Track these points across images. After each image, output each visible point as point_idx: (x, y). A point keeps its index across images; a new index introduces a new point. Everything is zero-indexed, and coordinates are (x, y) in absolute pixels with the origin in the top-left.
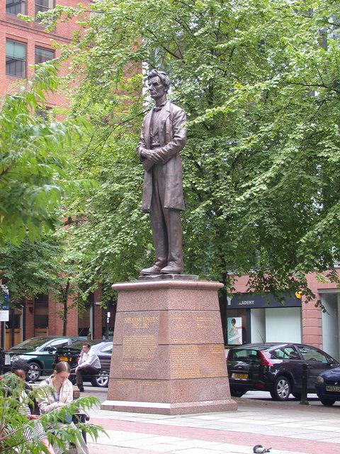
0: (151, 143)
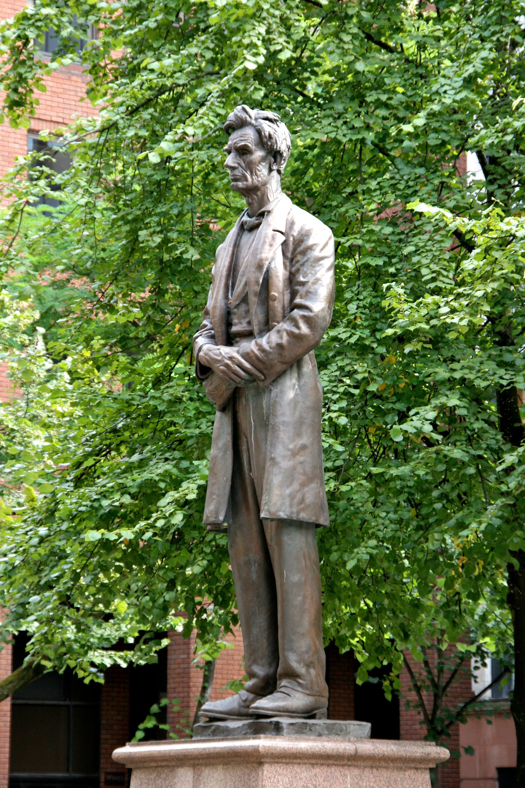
0: (229, 324)
